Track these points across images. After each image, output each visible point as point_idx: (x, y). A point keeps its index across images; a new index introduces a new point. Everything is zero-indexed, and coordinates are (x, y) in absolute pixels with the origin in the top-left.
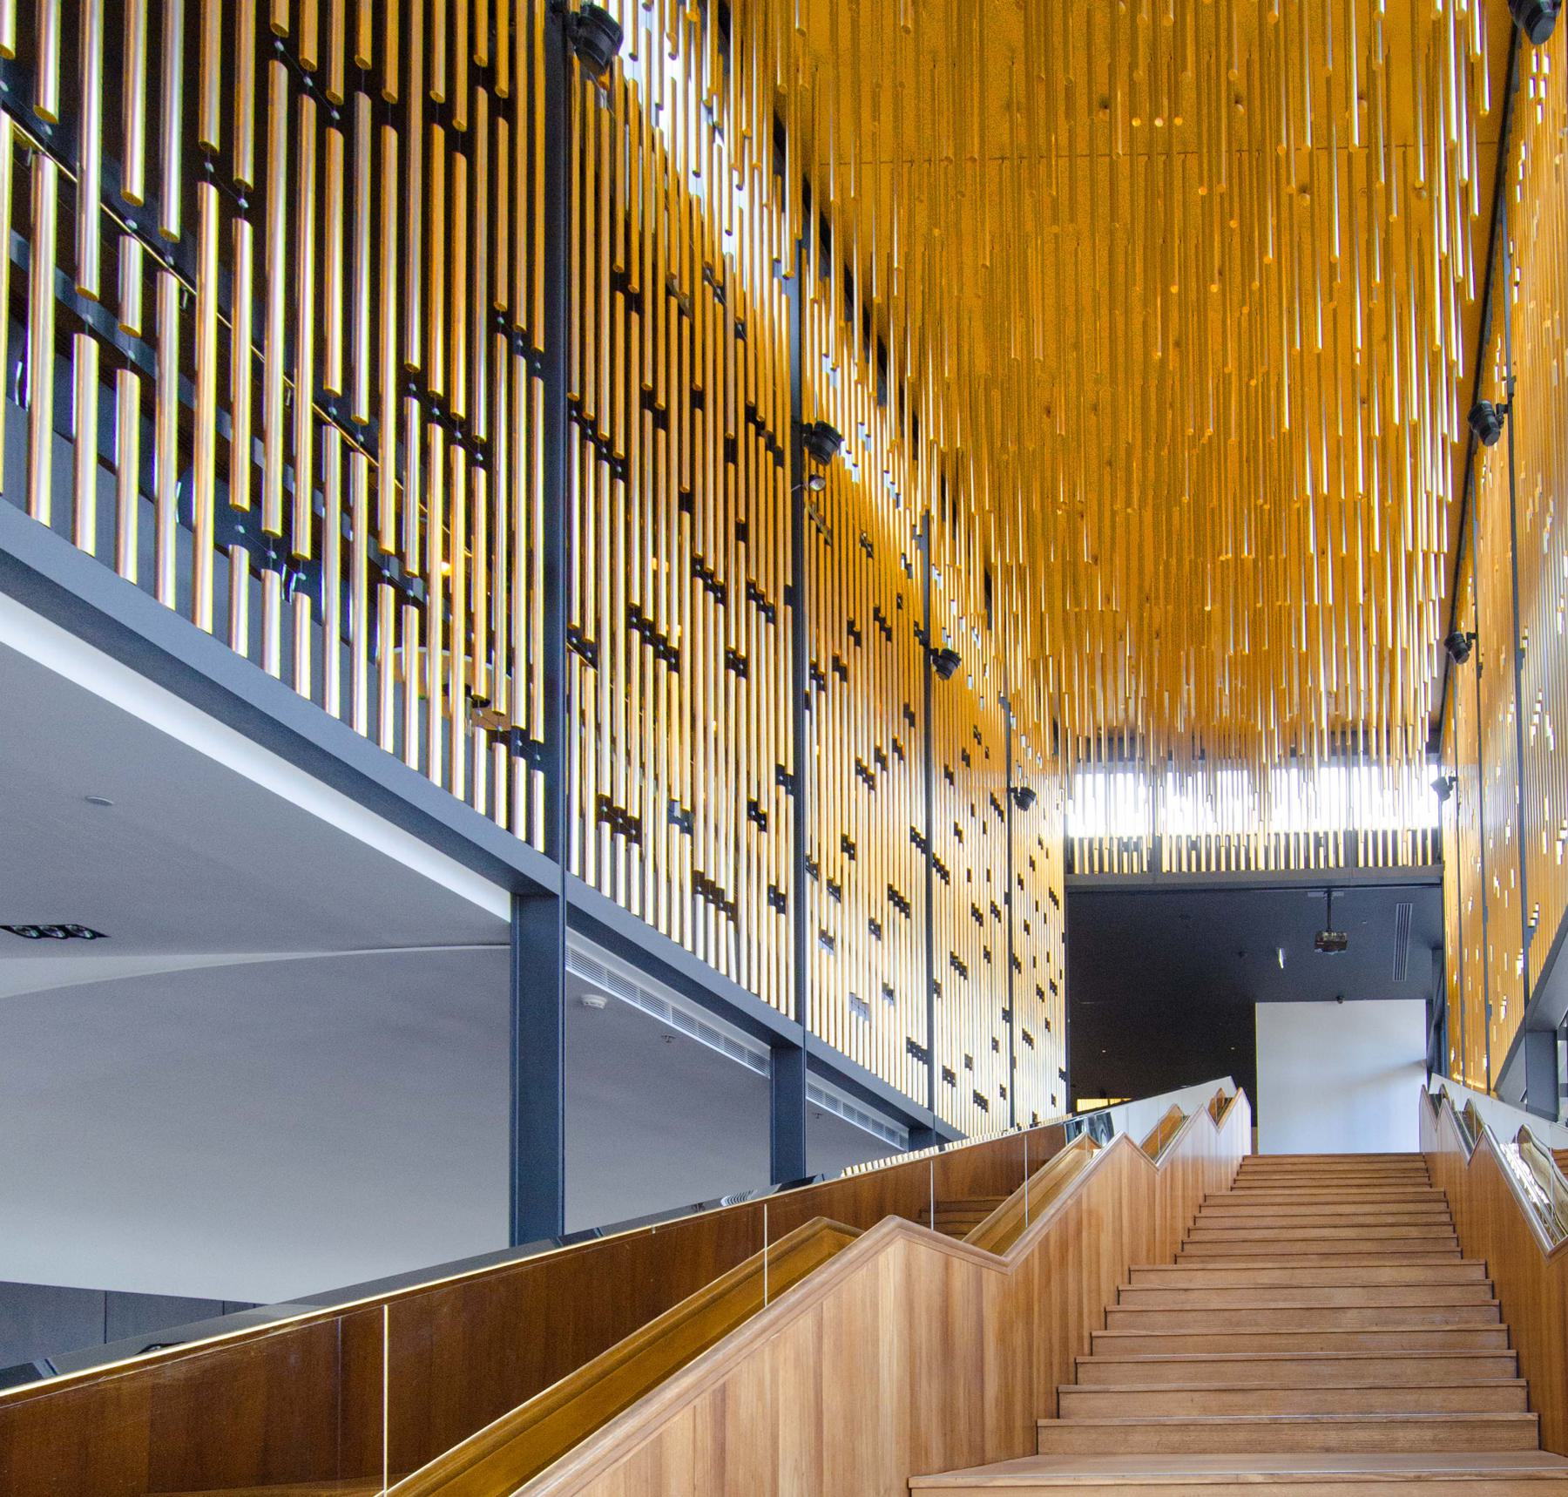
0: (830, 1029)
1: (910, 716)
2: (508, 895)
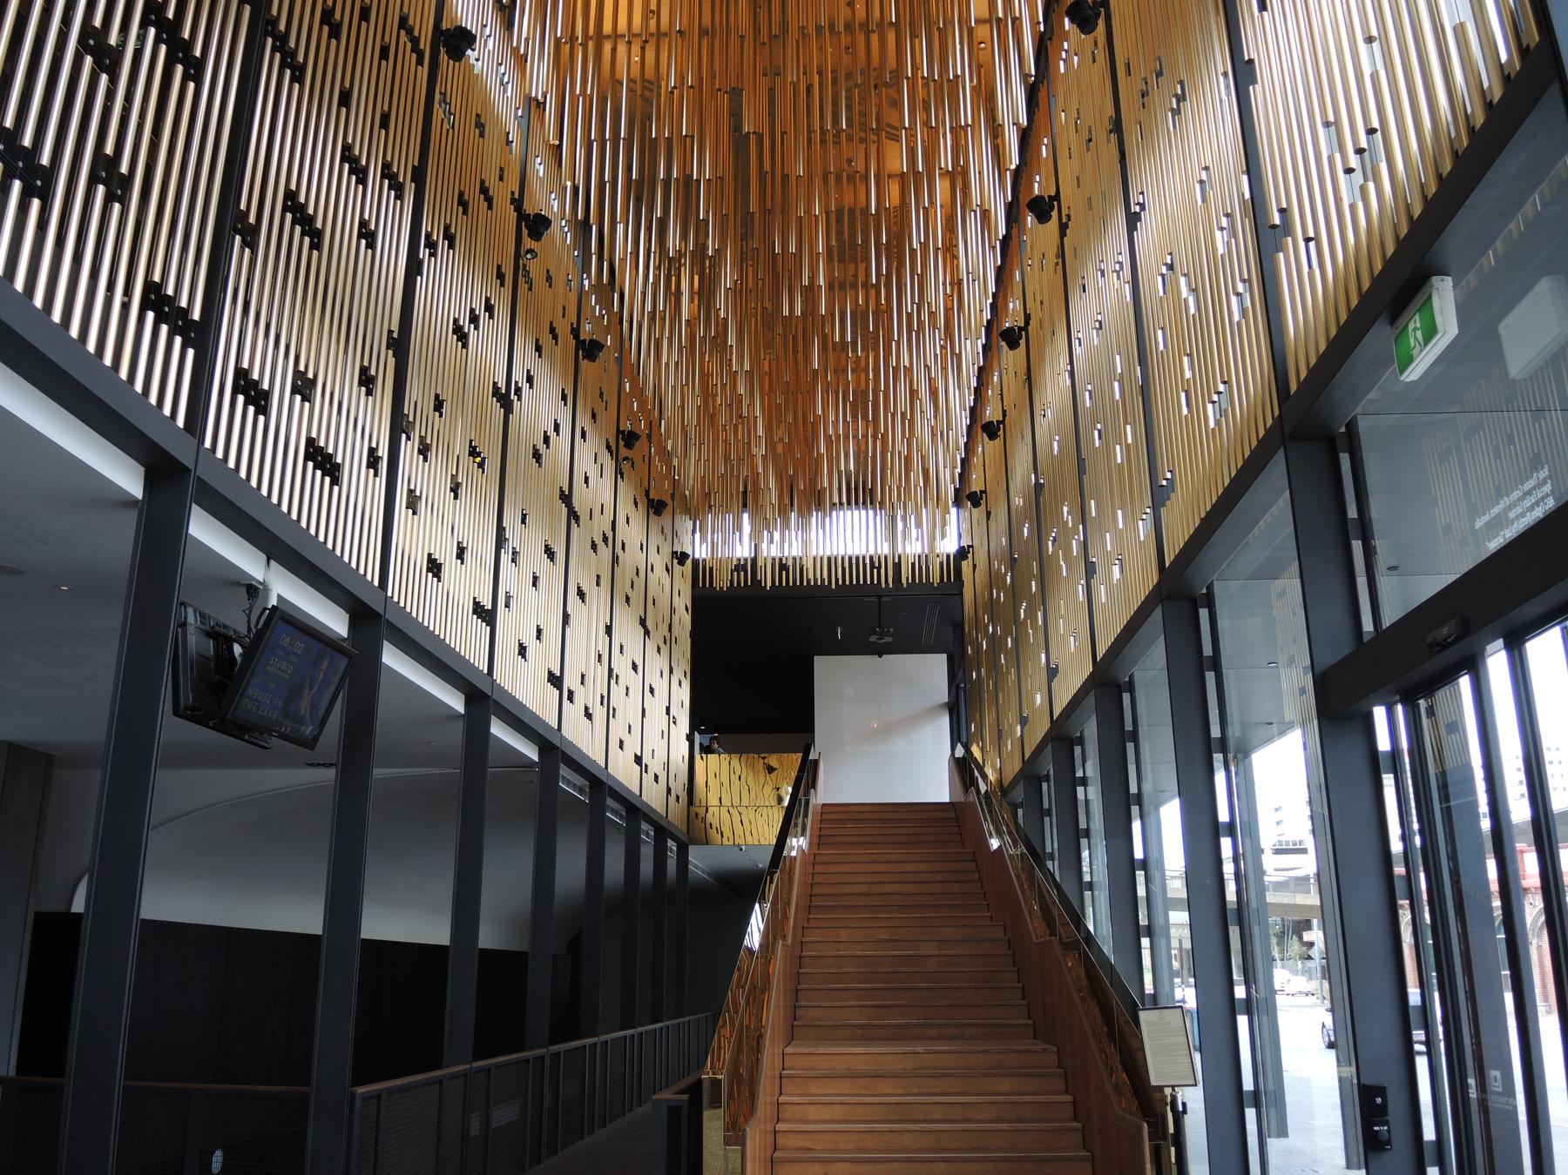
0: (412, 595)
1: (501, 276)
2: (141, 469)
